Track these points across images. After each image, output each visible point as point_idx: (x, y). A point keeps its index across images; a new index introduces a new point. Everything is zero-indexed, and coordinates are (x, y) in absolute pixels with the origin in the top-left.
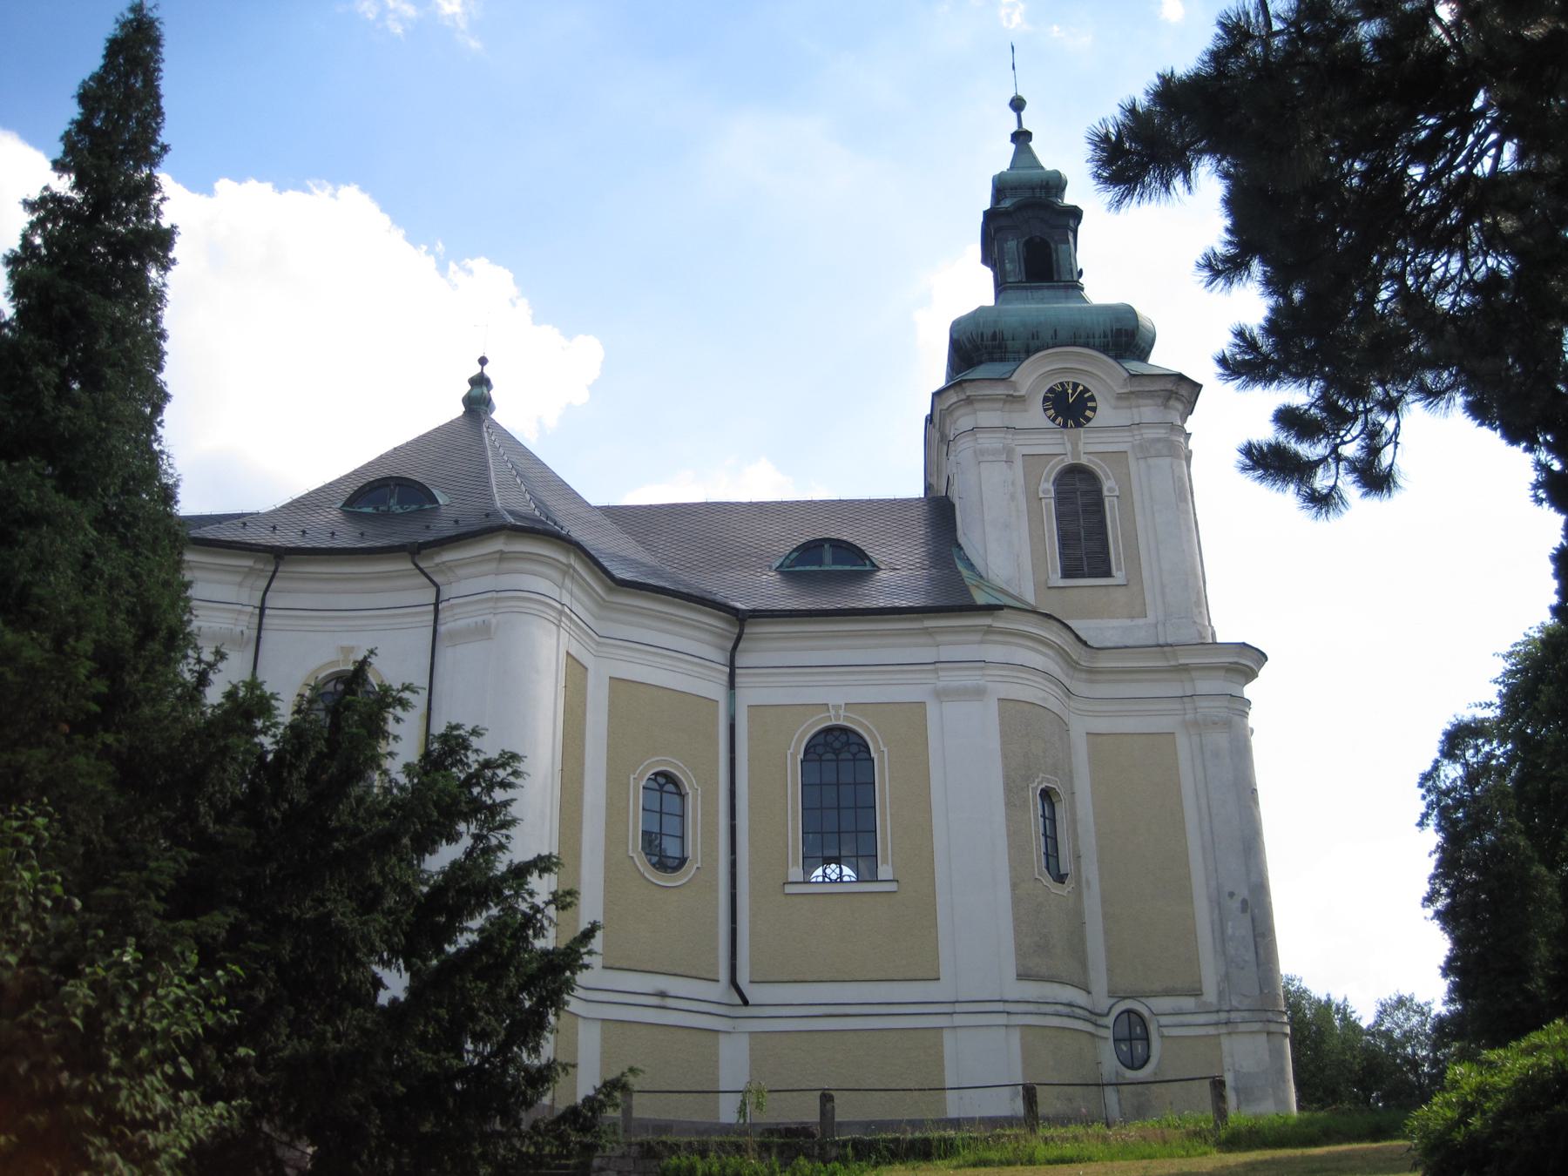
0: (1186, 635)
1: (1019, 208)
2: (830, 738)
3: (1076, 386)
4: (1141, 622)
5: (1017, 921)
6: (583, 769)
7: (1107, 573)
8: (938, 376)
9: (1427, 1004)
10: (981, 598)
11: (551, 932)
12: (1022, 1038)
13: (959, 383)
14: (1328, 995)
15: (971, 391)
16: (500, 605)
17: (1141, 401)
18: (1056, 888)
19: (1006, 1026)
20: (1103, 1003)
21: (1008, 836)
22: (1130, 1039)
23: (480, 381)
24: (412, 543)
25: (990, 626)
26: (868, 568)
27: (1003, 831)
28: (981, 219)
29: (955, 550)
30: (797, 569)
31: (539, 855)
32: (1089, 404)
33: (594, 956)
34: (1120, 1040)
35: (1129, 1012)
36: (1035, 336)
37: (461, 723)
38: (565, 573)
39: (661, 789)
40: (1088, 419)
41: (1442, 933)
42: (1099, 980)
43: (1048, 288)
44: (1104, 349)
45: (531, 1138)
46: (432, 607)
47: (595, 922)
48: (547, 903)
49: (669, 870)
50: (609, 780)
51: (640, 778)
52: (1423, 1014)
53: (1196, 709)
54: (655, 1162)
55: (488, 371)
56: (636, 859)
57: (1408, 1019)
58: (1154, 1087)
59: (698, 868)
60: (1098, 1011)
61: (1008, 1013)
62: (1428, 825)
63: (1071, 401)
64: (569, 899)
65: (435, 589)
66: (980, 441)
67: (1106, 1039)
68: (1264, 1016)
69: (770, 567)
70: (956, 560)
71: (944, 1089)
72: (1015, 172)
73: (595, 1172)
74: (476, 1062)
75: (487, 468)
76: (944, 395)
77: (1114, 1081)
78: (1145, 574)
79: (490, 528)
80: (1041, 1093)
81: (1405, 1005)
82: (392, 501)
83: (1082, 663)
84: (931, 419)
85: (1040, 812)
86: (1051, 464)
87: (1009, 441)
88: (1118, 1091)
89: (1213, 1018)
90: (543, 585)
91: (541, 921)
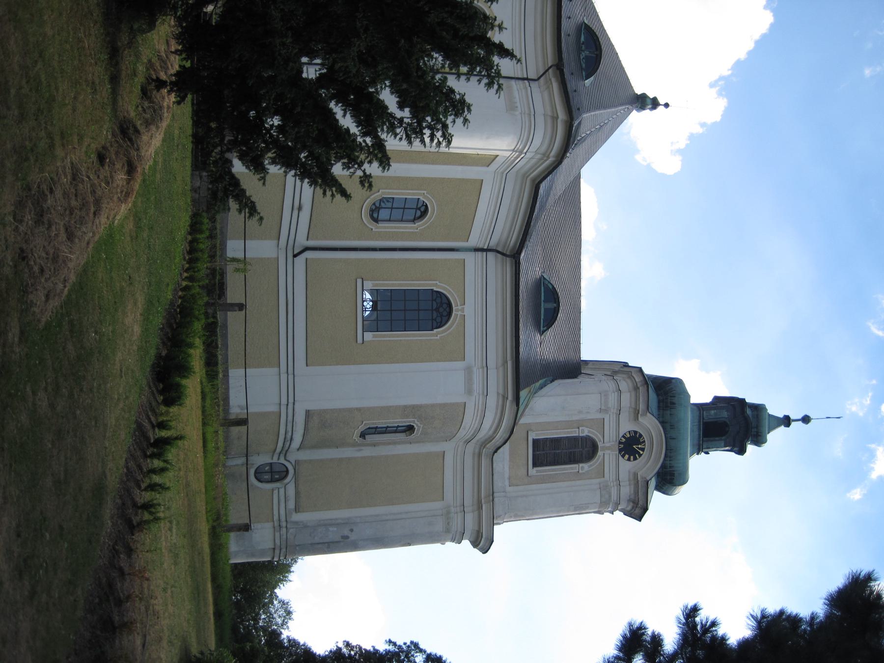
0: (498, 510)
1: (746, 419)
2: (445, 306)
3: (643, 450)
4: (507, 483)
5: (340, 411)
6: (430, 164)
7: (535, 465)
8: (649, 370)
9: (288, 628)
10: (523, 394)
11: (346, 173)
12: (273, 412)
13: (646, 383)
14: (293, 572)
15: (642, 390)
16: (526, 116)
17: (632, 487)
18: (357, 433)
19: (280, 404)
20: (293, 456)
21: (387, 406)
22: (272, 472)
23: (655, 104)
24: (563, 65)
25: (507, 398)
26: (542, 329)
27: (390, 404)
28: (740, 397)
29: (551, 378)
30: (542, 288)
31: (390, 158)
32: (632, 457)
33: (331, 198)
34: (271, 467)
35: (287, 471)
36: (672, 427)
37: (472, 112)
38: (544, 154)
39: (418, 209)
40: (623, 456)
41: (329, 650)
42: (304, 455)
43: (699, 435)
44: (663, 466)
45: (220, 158)
46: (525, 76)
47: (351, 197)
48: (364, 171)
49: (371, 213)
50: (423, 179)
51: (422, 195)
52: (282, 625)
53: (457, 513)
54: (205, 208)
55: (661, 108)
56: (378, 194)
57: (280, 617)
58: (245, 484)
59: (372, 229)
60: (288, 454)
61: (287, 405)
62: (389, 645)
63: (634, 446)
64: (367, 185)
65: (536, 78)
66: (613, 394)
67: (272, 459)
68: (283, 546)
69: (544, 272)
70: (544, 379)
71: (245, 368)
72: (767, 415)
73: (200, 173)
74: (266, 126)
75: (605, 108)
76: (640, 374)
77: (249, 462)
78: (534, 486)
79: (572, 111)
80: (243, 429)
81: (287, 615)
82: (588, 52)
83: (484, 450)
84: (625, 366)
85: (400, 425)
86: (599, 435)
87: (612, 410)
88: (243, 465)
89: (283, 518)
90: (537, 142)
91: (353, 166)
